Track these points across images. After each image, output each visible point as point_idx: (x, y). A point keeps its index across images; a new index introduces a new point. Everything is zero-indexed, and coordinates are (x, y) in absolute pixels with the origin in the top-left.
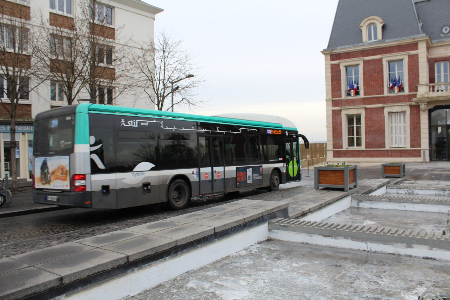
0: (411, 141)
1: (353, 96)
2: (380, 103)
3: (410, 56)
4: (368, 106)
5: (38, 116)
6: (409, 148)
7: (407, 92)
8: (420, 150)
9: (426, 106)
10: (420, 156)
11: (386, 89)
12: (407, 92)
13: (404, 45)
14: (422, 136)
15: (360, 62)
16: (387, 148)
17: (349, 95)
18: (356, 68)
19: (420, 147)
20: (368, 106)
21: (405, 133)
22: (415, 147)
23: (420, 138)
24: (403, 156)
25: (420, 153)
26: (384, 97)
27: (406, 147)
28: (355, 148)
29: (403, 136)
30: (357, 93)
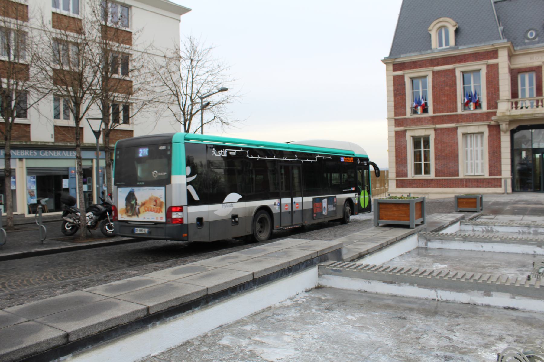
0: (489, 168)
1: (420, 114)
2: (453, 123)
4: (438, 126)
6: (487, 176)
7: (484, 108)
8: (501, 179)
9: (507, 126)
10: (500, 186)
12: (484, 108)
15: (428, 72)
16: (461, 176)
17: (415, 112)
18: (423, 80)
20: (438, 126)
21: (482, 159)
22: (494, 175)
23: (500, 165)
25: (501, 182)
27: (484, 175)
28: (423, 176)
29: (479, 162)
30: (425, 110)
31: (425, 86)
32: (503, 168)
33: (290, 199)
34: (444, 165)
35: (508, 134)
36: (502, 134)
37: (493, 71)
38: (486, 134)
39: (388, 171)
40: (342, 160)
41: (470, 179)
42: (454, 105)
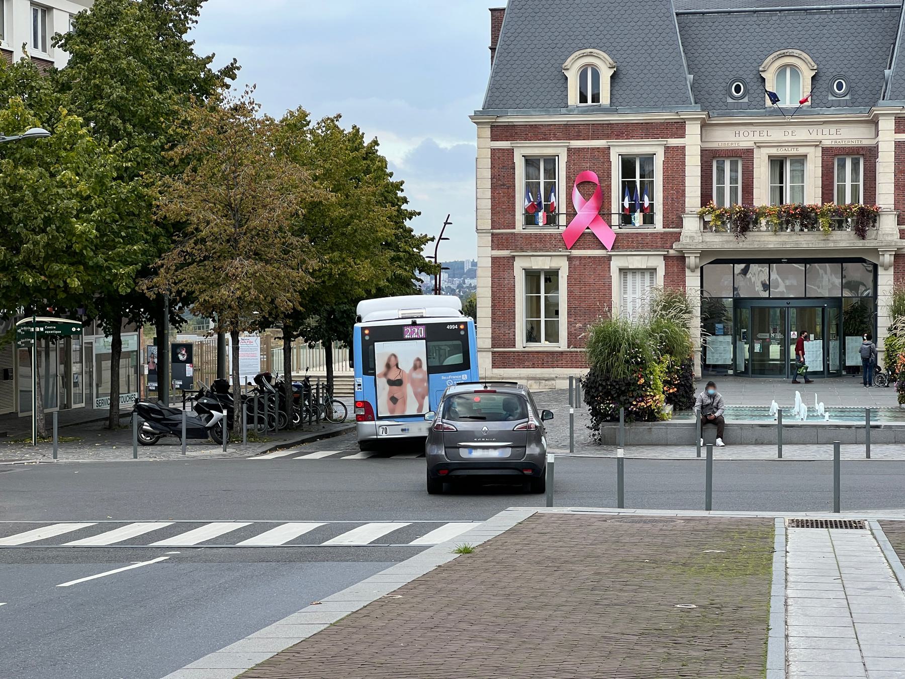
7: (659, 225)
9: (698, 260)
11: (520, 218)
12: (659, 225)
15: (559, 150)
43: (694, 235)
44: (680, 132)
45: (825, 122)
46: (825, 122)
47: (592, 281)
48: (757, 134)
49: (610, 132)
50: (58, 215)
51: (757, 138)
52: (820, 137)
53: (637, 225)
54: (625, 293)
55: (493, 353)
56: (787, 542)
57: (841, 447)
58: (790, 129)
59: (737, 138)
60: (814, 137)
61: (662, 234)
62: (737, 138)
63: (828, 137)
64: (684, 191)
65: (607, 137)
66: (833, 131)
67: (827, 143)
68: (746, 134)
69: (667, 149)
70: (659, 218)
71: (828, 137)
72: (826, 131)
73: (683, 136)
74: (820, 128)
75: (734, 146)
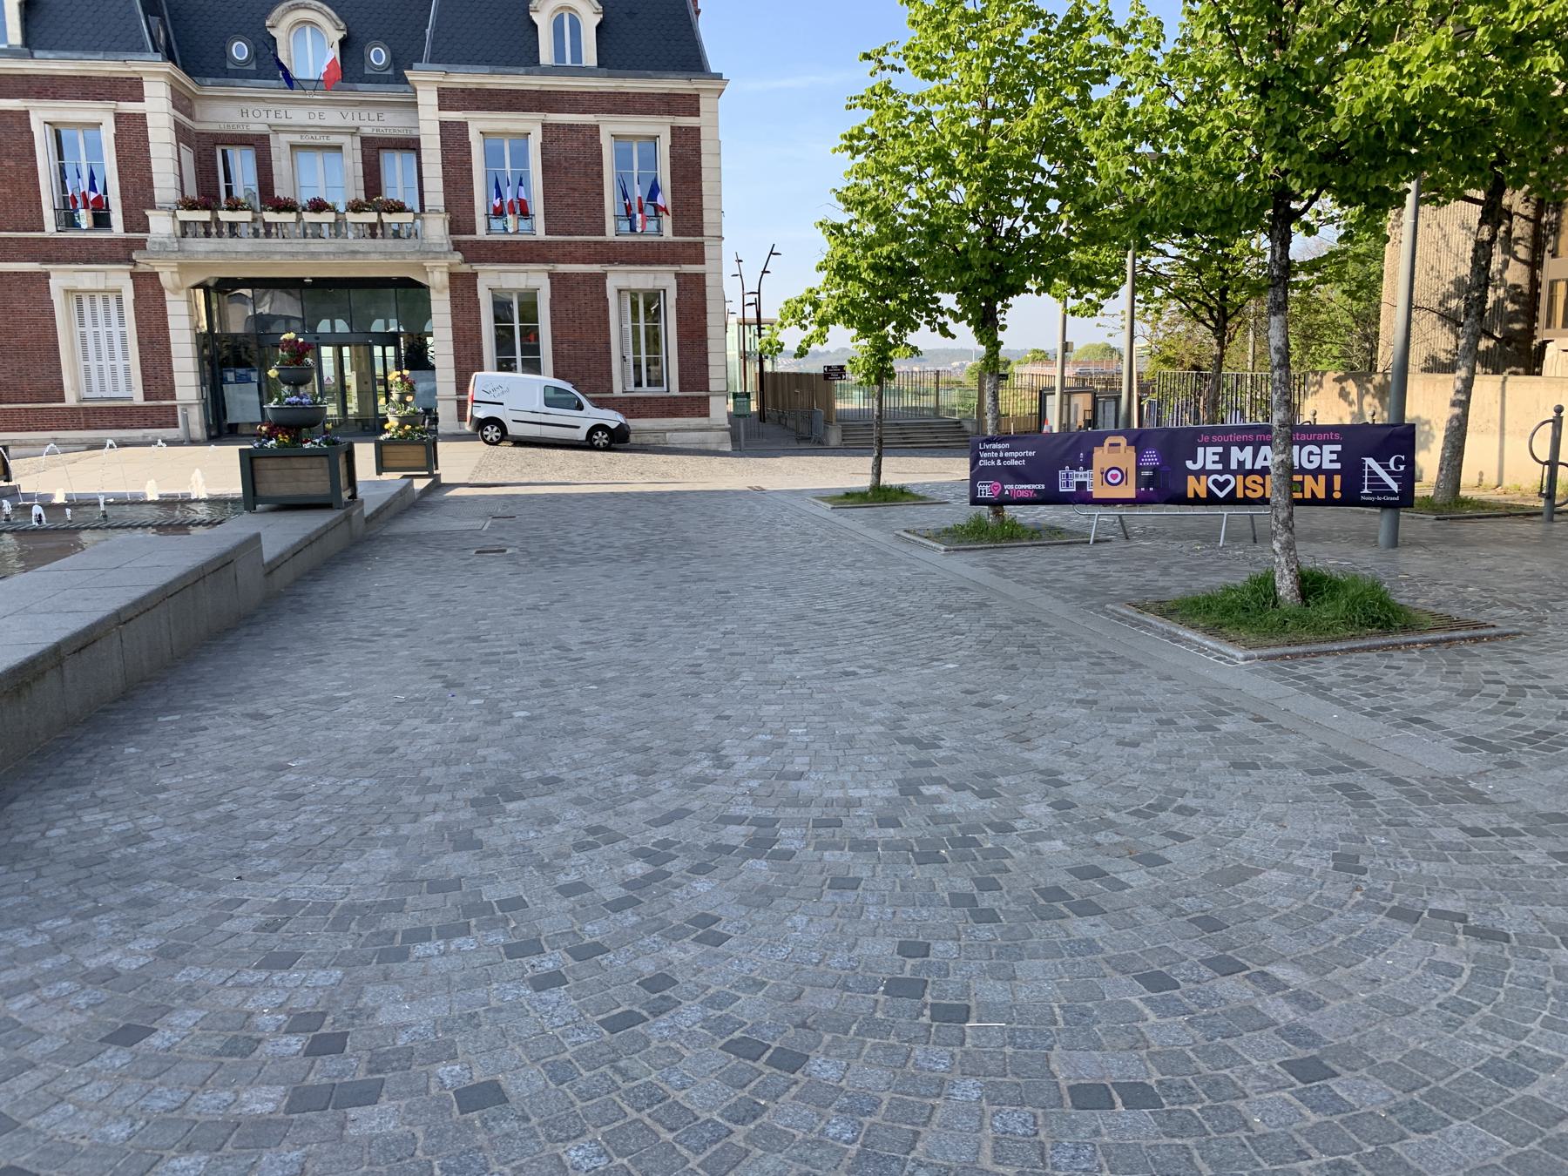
0: (143, 380)
1: (88, 230)
2: (34, 260)
3: (675, 131)
4: (562, 268)
5: (146, 217)
6: (138, 399)
7: (118, 228)
8: (175, 406)
9: (177, 276)
10: (176, 425)
11: (49, 215)
12: (118, 228)
13: (98, 78)
14: (176, 364)
15: (531, 124)
16: (71, 400)
17: (70, 221)
18: (90, 133)
19: (173, 397)
20: (562, 268)
21: (126, 357)
22: (157, 399)
23: (171, 371)
24: (643, 411)
25: (175, 414)
26: (46, 240)
27: (131, 399)
28: (646, 391)
29: (119, 363)
30: (101, 220)
31: (95, 150)
32: (178, 379)
33: (868, 462)
34: (20, 370)
35: (183, 295)
36: (168, 296)
37: (132, 134)
38: (129, 296)
39: (1539, 374)
40: (206, 352)
41: (95, 409)
42: (35, 211)
43: (166, 240)
44: (135, 93)
45: (361, 103)
46: (361, 103)
47: (22, 307)
48: (272, 114)
49: (26, 87)
50: (1018, 203)
51: (272, 120)
52: (357, 123)
53: (84, 226)
54: (82, 324)
55: (708, 390)
56: (1533, 434)
57: (325, 460)
58: (317, 109)
59: (244, 119)
60: (349, 122)
61: (123, 240)
62: (244, 119)
63: (367, 123)
64: (151, 179)
65: (24, 95)
66: (374, 116)
67: (367, 131)
68: (257, 114)
69: (119, 118)
70: (116, 217)
71: (367, 123)
72: (364, 115)
73: (140, 98)
74: (356, 110)
75: (242, 130)
